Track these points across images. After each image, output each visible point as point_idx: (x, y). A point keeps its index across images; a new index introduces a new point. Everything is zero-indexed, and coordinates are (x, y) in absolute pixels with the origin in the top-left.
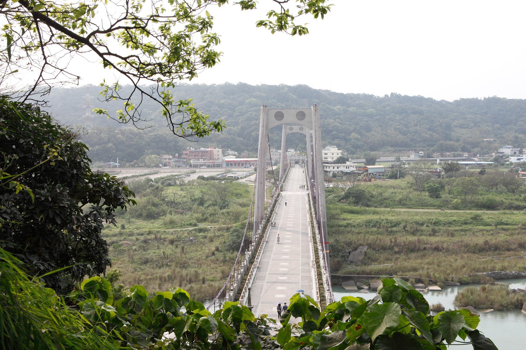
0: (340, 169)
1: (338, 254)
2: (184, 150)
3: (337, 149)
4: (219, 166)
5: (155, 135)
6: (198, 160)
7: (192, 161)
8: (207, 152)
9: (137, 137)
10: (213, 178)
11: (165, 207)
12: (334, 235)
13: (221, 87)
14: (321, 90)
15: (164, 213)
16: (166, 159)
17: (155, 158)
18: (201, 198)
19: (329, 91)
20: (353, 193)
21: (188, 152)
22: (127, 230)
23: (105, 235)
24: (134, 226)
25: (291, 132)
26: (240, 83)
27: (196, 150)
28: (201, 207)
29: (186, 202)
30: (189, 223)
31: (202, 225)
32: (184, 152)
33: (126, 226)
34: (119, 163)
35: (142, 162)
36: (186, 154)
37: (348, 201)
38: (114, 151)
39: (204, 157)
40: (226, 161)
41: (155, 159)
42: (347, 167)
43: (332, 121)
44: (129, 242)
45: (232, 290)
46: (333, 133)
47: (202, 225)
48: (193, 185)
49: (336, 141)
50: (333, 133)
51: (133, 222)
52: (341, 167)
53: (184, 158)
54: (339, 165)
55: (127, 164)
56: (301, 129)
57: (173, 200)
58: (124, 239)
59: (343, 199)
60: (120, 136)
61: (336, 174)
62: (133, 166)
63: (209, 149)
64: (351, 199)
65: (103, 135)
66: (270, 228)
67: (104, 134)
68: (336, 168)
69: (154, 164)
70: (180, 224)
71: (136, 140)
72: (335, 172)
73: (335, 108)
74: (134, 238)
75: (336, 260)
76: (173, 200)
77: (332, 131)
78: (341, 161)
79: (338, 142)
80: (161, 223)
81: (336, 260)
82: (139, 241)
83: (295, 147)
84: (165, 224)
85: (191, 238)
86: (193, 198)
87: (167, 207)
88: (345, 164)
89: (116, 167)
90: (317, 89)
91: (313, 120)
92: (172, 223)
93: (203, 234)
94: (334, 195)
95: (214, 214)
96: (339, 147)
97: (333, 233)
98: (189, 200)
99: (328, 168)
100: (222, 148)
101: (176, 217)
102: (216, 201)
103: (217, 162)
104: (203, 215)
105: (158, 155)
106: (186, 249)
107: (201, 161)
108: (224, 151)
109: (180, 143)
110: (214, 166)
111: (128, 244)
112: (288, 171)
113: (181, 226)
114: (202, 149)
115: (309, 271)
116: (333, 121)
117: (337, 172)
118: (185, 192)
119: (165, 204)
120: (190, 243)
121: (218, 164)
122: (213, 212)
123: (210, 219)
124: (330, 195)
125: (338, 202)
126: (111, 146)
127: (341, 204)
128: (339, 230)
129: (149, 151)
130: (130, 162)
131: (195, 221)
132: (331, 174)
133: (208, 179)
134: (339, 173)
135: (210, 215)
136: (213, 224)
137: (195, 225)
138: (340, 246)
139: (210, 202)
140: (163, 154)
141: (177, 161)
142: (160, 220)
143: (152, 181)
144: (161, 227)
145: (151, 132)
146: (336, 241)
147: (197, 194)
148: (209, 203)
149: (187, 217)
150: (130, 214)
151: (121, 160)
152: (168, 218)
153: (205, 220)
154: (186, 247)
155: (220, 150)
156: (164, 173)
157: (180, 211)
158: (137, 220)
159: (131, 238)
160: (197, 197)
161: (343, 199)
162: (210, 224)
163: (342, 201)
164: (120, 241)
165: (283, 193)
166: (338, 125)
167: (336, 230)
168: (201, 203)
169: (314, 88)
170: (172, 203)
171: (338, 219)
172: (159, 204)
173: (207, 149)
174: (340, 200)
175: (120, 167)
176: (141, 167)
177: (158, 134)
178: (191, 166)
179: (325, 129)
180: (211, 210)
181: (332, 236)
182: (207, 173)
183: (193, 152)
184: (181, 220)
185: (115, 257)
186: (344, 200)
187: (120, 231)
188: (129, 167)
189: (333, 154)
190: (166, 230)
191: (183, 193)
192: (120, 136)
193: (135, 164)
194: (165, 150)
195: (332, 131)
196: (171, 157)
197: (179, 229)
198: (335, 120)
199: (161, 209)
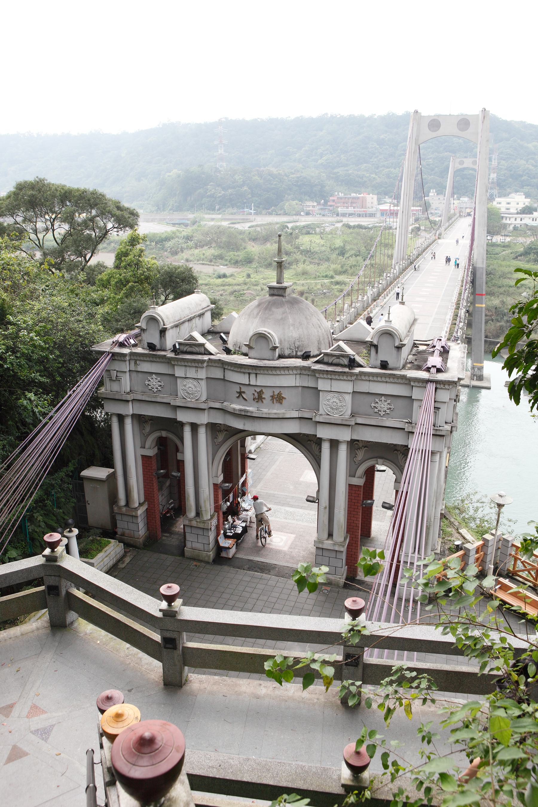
0: (523, 222)
1: (502, 318)
2: (331, 196)
3: (524, 196)
4: (372, 215)
5: (298, 178)
6: (347, 207)
7: (339, 209)
8: (358, 198)
9: (277, 179)
10: (360, 227)
11: (298, 256)
12: (501, 296)
13: (383, 118)
14: (513, 121)
15: (297, 261)
16: (309, 206)
17: (297, 204)
18: (342, 247)
19: (525, 122)
20: (535, 249)
21: (335, 198)
22: (253, 280)
23: (228, 284)
24: (262, 276)
25: (461, 167)
26: (407, 112)
27: (345, 196)
28: (341, 257)
29: (325, 251)
30: (324, 275)
31: (338, 278)
32: (331, 198)
33: (252, 276)
34: (254, 210)
35: (281, 210)
36: (334, 201)
37: (527, 259)
38: (250, 196)
39: (354, 205)
40: (381, 210)
41: (296, 206)
42: (533, 219)
43: (523, 162)
44: (252, 292)
45: (338, 321)
46: (523, 178)
47: (338, 278)
48: (335, 234)
49: (526, 189)
50: (523, 178)
51: (261, 272)
52: (525, 219)
53: (331, 206)
54: (524, 216)
55: (264, 212)
56: (475, 163)
57: (309, 249)
58: (248, 289)
59: (521, 255)
60: (257, 177)
61: (518, 227)
62: (270, 214)
63: (362, 195)
64: (532, 256)
65: (237, 177)
66: (411, 272)
67: (239, 176)
68: (518, 221)
69: (294, 212)
70: (314, 276)
71: (275, 183)
72: (517, 225)
73: (530, 146)
74: (259, 288)
75: (498, 324)
76: (309, 249)
77: (521, 176)
78: (526, 211)
79: (527, 190)
80: (292, 274)
81: (498, 324)
82: (264, 291)
83: (470, 196)
84: (297, 275)
85: (324, 291)
86: (333, 247)
87: (301, 256)
88: (531, 216)
89: (251, 214)
90: (509, 120)
91: (480, 130)
92: (304, 273)
93: (339, 287)
94: (510, 251)
95: (355, 266)
96: (527, 196)
97: (501, 294)
98: (329, 250)
99: (508, 219)
100: (378, 194)
101: (310, 268)
102: (359, 251)
103: (370, 211)
104: (342, 267)
105: (300, 200)
106: (317, 302)
107: (351, 210)
108: (380, 199)
109: (327, 188)
110: (366, 216)
111: (252, 294)
112: (455, 220)
113: (315, 278)
114: (353, 195)
115: (446, 314)
116: (525, 162)
117: (519, 226)
118: (323, 241)
119: (299, 253)
120: (322, 296)
121: (371, 214)
122: (354, 263)
123: (350, 271)
124: (504, 250)
125: (514, 259)
126: (246, 190)
127: (517, 262)
128: (508, 291)
129: (289, 197)
130: (267, 209)
131: (331, 273)
132: (511, 228)
133: (354, 227)
134: (523, 226)
135: (351, 267)
136: (353, 277)
137: (332, 277)
138: (507, 309)
139: (353, 252)
140: (306, 200)
141: (322, 209)
142: (291, 271)
143: (288, 228)
144: (292, 278)
145: (293, 174)
146: (503, 302)
147: (338, 243)
148: (351, 253)
149: (324, 266)
150: (258, 263)
151: (257, 207)
152: (301, 267)
153: (345, 272)
154: (316, 300)
155: (375, 197)
156: (303, 221)
157: (317, 261)
158: (266, 270)
159: (256, 287)
160: (337, 246)
161: (521, 255)
162: (349, 277)
163: (519, 258)
164: (243, 290)
165: (440, 241)
166: (531, 167)
167: (504, 291)
168: (342, 252)
169: (504, 118)
170: (308, 253)
171: (510, 278)
172: (291, 252)
173: (360, 196)
174: (517, 257)
175: (256, 214)
176: (280, 215)
177: (301, 176)
178: (338, 215)
179: (512, 173)
180: (352, 261)
181: (498, 297)
182: (353, 221)
183: (341, 198)
184: (316, 271)
185: (235, 307)
186: (523, 257)
187: (245, 281)
188: (266, 214)
189: (518, 204)
190: (297, 282)
191: (322, 242)
192: (257, 177)
193: (273, 211)
194: (309, 196)
195: (521, 176)
196: (315, 204)
197: (313, 281)
198: (527, 162)
199: (293, 258)
